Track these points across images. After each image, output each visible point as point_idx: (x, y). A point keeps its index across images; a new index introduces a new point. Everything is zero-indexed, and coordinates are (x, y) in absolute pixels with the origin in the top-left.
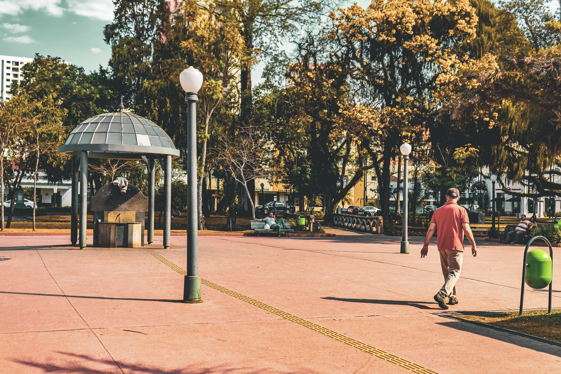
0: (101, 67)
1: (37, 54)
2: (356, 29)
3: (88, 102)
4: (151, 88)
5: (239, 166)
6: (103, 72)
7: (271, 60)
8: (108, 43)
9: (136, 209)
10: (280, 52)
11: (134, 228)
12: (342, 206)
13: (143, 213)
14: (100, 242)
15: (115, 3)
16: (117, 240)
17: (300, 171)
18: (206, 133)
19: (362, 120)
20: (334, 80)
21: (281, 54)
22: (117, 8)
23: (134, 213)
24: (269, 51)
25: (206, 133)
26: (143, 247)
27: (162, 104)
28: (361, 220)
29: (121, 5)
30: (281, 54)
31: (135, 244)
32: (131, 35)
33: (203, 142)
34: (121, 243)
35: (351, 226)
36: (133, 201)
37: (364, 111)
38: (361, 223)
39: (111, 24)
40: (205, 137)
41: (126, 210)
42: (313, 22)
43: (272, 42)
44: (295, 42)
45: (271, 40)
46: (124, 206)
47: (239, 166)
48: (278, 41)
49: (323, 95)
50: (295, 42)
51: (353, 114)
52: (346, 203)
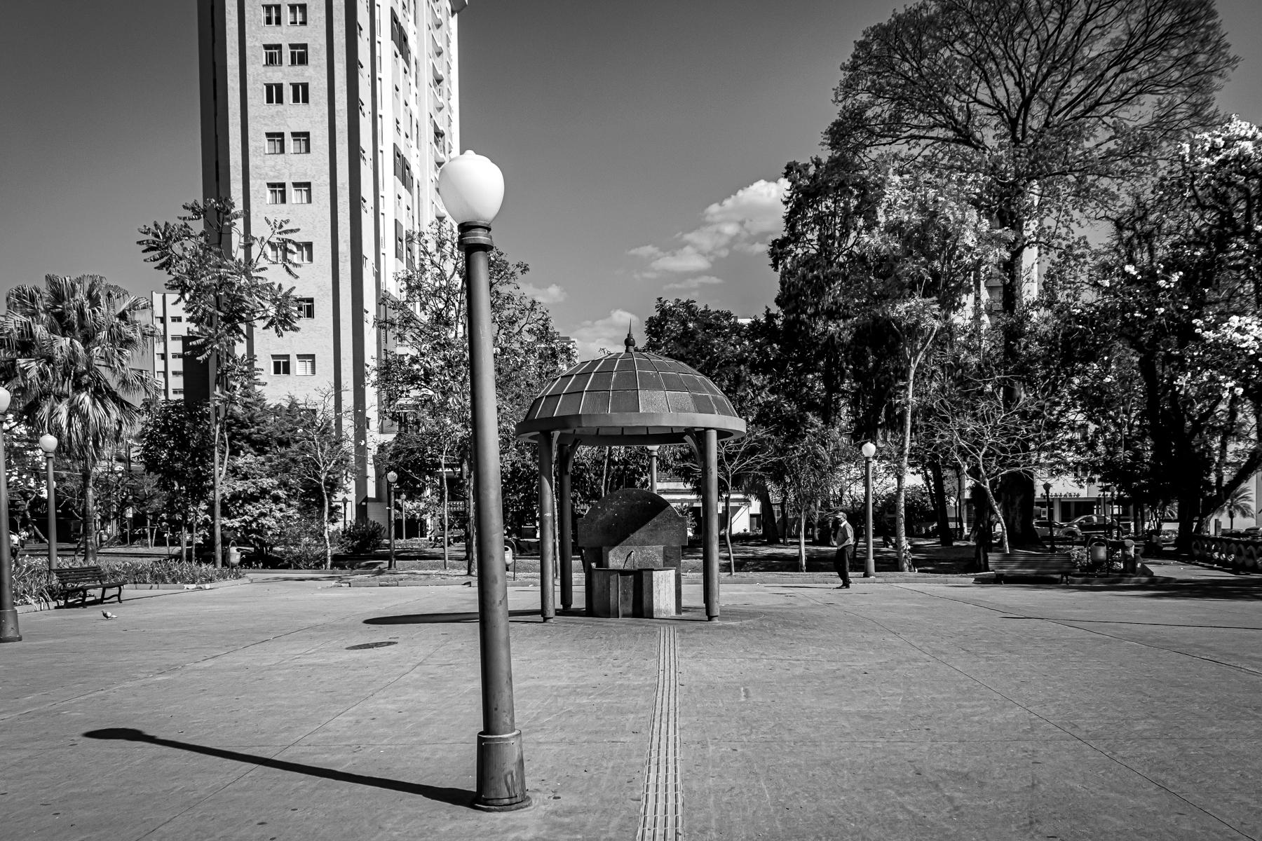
0: (769, 310)
1: (660, 299)
2: (1231, 167)
3: (738, 366)
4: (840, 334)
5: (975, 452)
6: (770, 317)
7: (1059, 256)
8: (776, 269)
9: (664, 540)
10: (1076, 240)
11: (654, 579)
12: (1220, 522)
13: (676, 548)
14: (595, 606)
15: (786, 203)
16: (622, 603)
17: (1130, 457)
18: (910, 396)
19: (1244, 345)
20: (1181, 273)
21: (1078, 243)
22: (789, 210)
23: (661, 548)
24: (1055, 242)
25: (910, 396)
26: (679, 616)
27: (859, 359)
28: (1246, 547)
29: (795, 203)
30: (1078, 243)
31: (660, 611)
32: (813, 251)
33: (904, 413)
34: (630, 610)
35: (1226, 559)
36: (656, 525)
37: (1249, 328)
38: (1245, 552)
39: (780, 238)
40: (908, 403)
41: (643, 543)
42: (1142, 173)
43: (1060, 224)
44: (1108, 218)
45: (1058, 222)
46: (638, 535)
47: (975, 452)
48: (1072, 221)
49: (1160, 306)
50: (1108, 218)
51: (1225, 335)
52: (1238, 516)
